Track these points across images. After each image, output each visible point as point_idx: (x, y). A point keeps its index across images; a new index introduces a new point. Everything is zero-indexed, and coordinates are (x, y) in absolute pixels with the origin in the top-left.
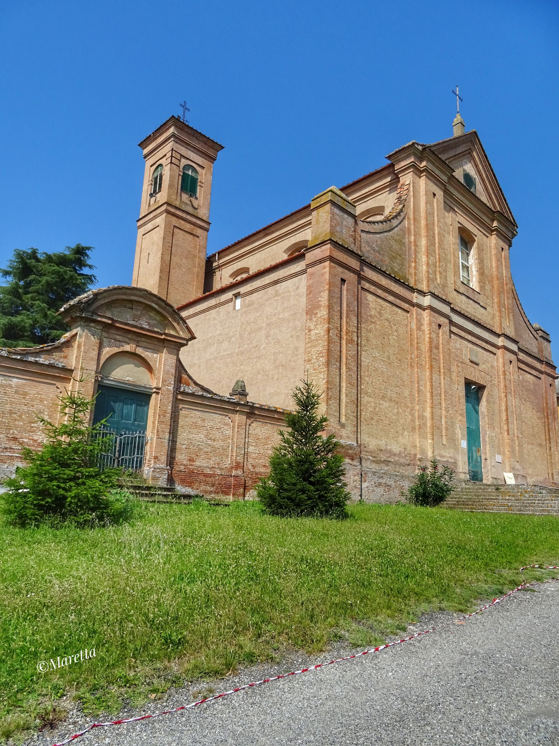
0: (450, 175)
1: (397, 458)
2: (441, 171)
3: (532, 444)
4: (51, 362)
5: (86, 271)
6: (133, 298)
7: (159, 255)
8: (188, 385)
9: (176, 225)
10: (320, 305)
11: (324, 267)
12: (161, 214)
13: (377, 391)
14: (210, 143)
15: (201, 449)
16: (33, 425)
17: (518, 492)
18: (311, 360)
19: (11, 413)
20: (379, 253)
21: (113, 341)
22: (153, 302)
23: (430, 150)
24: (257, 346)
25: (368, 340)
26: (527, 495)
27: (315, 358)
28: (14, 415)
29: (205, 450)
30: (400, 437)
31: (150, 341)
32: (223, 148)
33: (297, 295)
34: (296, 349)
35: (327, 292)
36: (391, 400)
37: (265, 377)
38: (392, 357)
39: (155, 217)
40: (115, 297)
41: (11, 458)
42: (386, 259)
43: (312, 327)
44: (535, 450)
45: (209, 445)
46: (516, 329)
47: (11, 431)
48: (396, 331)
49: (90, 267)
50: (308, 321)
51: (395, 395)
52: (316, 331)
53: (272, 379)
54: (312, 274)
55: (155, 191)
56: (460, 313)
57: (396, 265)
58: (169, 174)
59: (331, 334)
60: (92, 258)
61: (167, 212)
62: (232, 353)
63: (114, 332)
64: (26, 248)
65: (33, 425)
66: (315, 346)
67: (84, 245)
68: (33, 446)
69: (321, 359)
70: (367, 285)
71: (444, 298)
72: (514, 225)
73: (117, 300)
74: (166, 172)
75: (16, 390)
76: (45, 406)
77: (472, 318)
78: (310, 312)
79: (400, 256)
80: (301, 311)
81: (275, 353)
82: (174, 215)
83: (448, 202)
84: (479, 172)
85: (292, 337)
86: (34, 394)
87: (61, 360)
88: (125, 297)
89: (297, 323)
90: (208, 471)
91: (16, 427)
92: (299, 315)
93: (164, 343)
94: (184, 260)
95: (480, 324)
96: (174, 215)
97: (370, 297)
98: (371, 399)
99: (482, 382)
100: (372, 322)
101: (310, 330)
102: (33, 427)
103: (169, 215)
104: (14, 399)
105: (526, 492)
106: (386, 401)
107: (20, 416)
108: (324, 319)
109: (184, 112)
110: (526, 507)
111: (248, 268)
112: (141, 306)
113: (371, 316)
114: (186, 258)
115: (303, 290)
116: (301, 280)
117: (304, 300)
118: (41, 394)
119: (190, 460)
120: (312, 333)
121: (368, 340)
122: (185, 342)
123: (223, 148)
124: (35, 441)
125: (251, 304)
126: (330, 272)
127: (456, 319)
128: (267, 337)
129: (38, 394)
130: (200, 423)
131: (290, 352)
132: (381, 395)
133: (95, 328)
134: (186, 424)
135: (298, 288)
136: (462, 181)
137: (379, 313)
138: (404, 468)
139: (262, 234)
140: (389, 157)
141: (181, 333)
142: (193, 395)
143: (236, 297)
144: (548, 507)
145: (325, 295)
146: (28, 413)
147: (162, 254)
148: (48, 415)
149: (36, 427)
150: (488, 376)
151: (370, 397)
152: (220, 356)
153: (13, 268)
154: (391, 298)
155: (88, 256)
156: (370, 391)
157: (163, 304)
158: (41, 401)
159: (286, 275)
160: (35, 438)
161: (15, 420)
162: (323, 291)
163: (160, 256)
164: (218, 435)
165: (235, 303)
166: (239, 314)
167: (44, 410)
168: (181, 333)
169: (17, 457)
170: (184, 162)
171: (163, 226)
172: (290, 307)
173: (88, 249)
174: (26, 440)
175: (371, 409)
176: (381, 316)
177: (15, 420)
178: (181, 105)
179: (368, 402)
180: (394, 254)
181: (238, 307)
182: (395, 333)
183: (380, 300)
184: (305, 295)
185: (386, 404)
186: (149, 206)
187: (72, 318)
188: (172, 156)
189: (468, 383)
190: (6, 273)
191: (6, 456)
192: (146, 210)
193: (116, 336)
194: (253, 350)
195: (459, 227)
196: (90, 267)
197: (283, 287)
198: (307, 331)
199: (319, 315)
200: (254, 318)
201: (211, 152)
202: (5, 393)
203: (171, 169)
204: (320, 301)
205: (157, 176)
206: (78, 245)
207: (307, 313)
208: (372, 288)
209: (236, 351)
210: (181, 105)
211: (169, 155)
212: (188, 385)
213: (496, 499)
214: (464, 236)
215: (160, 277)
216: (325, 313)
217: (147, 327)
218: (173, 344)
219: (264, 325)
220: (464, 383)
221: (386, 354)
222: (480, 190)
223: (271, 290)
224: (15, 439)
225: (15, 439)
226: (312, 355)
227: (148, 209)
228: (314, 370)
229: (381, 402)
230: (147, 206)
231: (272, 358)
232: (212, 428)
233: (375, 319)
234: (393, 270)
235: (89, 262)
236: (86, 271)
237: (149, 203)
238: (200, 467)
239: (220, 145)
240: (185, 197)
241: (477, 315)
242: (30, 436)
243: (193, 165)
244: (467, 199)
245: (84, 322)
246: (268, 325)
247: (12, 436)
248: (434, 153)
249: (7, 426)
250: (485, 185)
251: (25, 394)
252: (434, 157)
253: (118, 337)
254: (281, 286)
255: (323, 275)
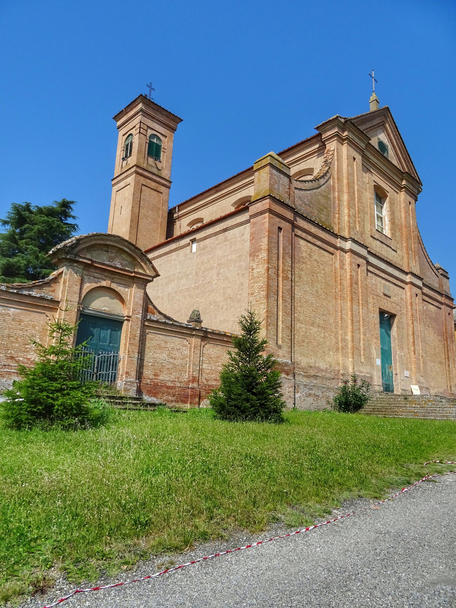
0: (367, 143)
1: (323, 374)
2: (360, 139)
3: (434, 362)
4: (42, 295)
5: (70, 221)
6: (108, 243)
7: (130, 208)
8: (154, 314)
9: (144, 183)
10: (261, 249)
11: (265, 218)
12: (131, 174)
13: (307, 319)
14: (171, 117)
15: (164, 366)
16: (27, 346)
17: (422, 401)
18: (253, 294)
19: (9, 336)
20: (310, 206)
21: (92, 278)
22: (125, 246)
23: (351, 122)
24: (209, 282)
25: (300, 278)
26: (430, 404)
27: (257, 291)
28: (12, 339)
29: (168, 366)
30: (327, 356)
31: (123, 278)
32: (182, 120)
33: (242, 240)
34: (242, 284)
35: (267, 238)
36: (319, 326)
37: (217, 308)
38: (320, 291)
39: (127, 177)
40: (93, 242)
41: (9, 373)
42: (315, 211)
43: (255, 267)
44: (436, 367)
45: (171, 363)
46: (421, 268)
47: (9, 352)
48: (323, 270)
49: (74, 217)
50: (252, 261)
51: (322, 322)
52: (258, 270)
53: (222, 309)
54: (254, 224)
55: (126, 156)
56: (375, 255)
57: (323, 216)
58: (138, 142)
59: (270, 272)
60: (75, 210)
61: (137, 172)
62: (189, 288)
63: (93, 270)
64: (22, 202)
65: (27, 346)
66: (257, 282)
67: (68, 199)
68: (27, 363)
69: (262, 293)
70: (299, 233)
71: (362, 243)
72: (419, 183)
73: (96, 244)
74: (136, 140)
75: (13, 318)
76: (37, 331)
77: (385, 259)
78: (253, 254)
79: (326, 209)
80: (245, 253)
81: (224, 288)
82: (142, 175)
83: (365, 165)
84: (391, 140)
85: (238, 275)
86: (28, 321)
87: (50, 293)
88: (102, 242)
89: (243, 263)
90: (170, 384)
91: (13, 348)
92: (244, 257)
93: (134, 279)
94: (150, 212)
95: (391, 264)
96: (142, 175)
97: (302, 242)
98: (303, 326)
99: (393, 311)
100: (303, 263)
101: (253, 269)
102: (27, 348)
103: (138, 176)
104: (12, 325)
105: (429, 401)
106: (315, 327)
107: (17, 339)
108: (264, 260)
109: (150, 91)
110: (429, 413)
111: (203, 219)
112: (115, 250)
113: (302, 257)
114: (152, 210)
115: (247, 236)
116: (246, 228)
117: (248, 244)
118: (33, 321)
119: (155, 375)
120: (255, 271)
121: (300, 278)
122: (151, 279)
123: (182, 120)
124: (29, 359)
125: (205, 248)
126: (269, 221)
127: (372, 260)
128: (218, 274)
129: (31, 321)
130: (163, 344)
131: (236, 287)
132: (311, 322)
133: (77, 267)
134: (152, 345)
135: (243, 235)
136: (377, 147)
137: (310, 255)
138: (330, 382)
139: (213, 191)
140: (317, 128)
141: (148, 272)
142: (157, 322)
143: (192, 242)
144: (447, 413)
145: (265, 240)
146: (23, 337)
147: (132, 207)
148: (39, 338)
149: (29, 348)
150: (398, 307)
151: (302, 323)
152: (180, 290)
153: (11, 218)
154: (319, 243)
155: (72, 209)
156: (301, 319)
157: (133, 248)
158: (34, 327)
159: (233, 224)
160: (29, 357)
161: (12, 342)
162: (264, 237)
163: (131, 208)
164: (178, 355)
165: (192, 247)
166: (195, 256)
167: (36, 334)
168: (148, 272)
169: (14, 372)
170: (150, 132)
171: (133, 184)
172: (237, 250)
173: (72, 203)
174: (21, 359)
175: (302, 333)
176: (311, 257)
177: (12, 342)
178: (147, 85)
179: (300, 328)
180: (321, 207)
181: (194, 250)
182: (322, 272)
183: (310, 245)
184: (249, 241)
185: (315, 330)
186: (122, 168)
187: (59, 259)
188: (140, 127)
189: (382, 312)
190: (5, 223)
191: (5, 371)
192: (119, 171)
193: (94, 274)
194: (206, 285)
195: (374, 185)
196: (74, 217)
197: (231, 234)
198: (250, 270)
199: (260, 257)
200: (207, 259)
201: (172, 124)
202: (4, 320)
203: (139, 138)
204: (261, 245)
205: (128, 144)
206: (64, 199)
207: (250, 255)
208: (304, 235)
209: (193, 286)
210: (147, 85)
211: (138, 126)
212: (154, 314)
213: (405, 407)
214: (379, 192)
215: (131, 226)
216: (265, 255)
217: (120, 266)
218: (141, 280)
219: (215, 265)
220: (378, 312)
221: (315, 288)
222: (391, 155)
223: (221, 236)
224: (12, 358)
225: (12, 358)
226: (254, 289)
227: (121, 171)
228: (256, 302)
229: (311, 328)
230: (120, 168)
231: (222, 292)
232: (173, 349)
233: (306, 260)
234: (321, 220)
235: (72, 214)
236: (70, 221)
237: (122, 166)
238: (163, 380)
239: (180, 119)
240: (151, 160)
241: (389, 256)
242: (24, 355)
243: (158, 134)
244: (381, 162)
245: (69, 263)
246: (219, 265)
247: (10, 355)
248: (354, 125)
249: (6, 347)
250: (396, 151)
251: (21, 321)
252: (354, 128)
253: (96, 275)
254: (229, 233)
255: (263, 224)
